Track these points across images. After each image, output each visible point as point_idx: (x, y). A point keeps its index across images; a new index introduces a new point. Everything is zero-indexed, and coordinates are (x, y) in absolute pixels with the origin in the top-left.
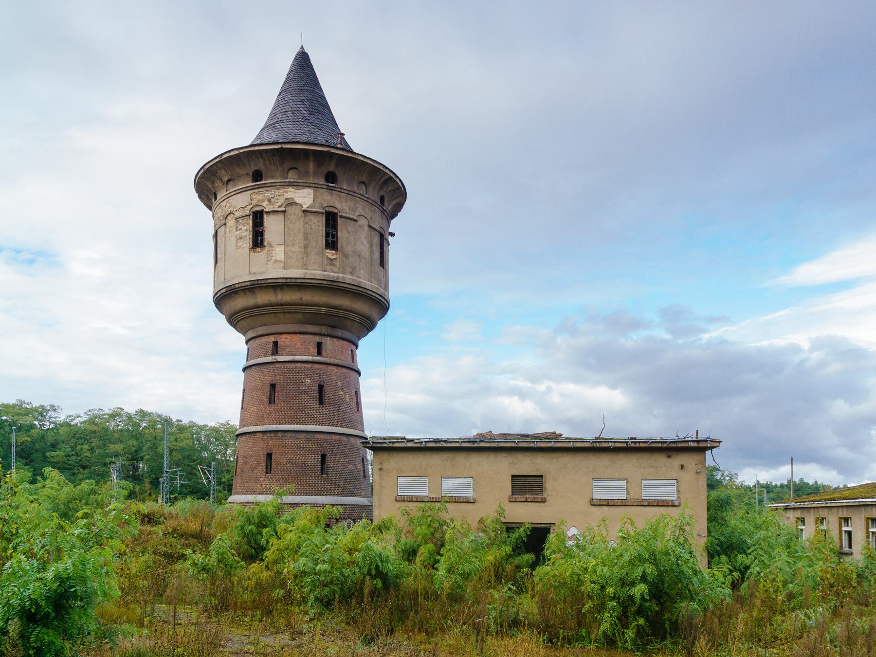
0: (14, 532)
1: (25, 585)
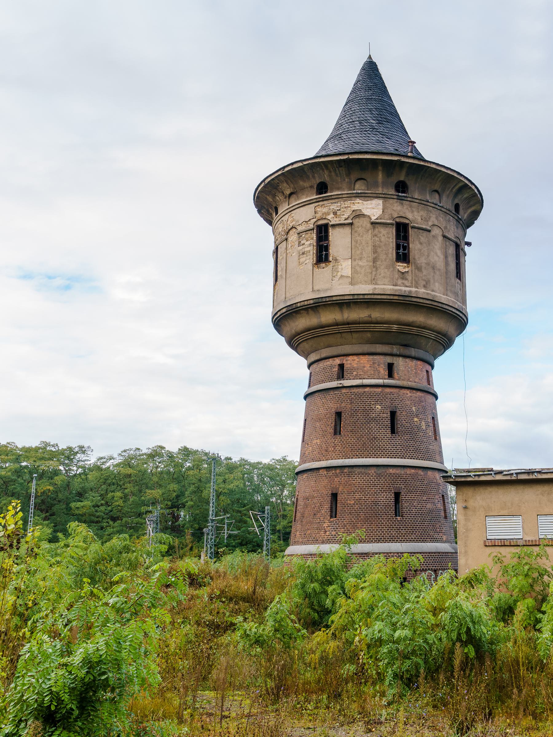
0: (30, 604)
1: (46, 674)
